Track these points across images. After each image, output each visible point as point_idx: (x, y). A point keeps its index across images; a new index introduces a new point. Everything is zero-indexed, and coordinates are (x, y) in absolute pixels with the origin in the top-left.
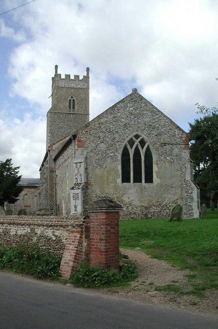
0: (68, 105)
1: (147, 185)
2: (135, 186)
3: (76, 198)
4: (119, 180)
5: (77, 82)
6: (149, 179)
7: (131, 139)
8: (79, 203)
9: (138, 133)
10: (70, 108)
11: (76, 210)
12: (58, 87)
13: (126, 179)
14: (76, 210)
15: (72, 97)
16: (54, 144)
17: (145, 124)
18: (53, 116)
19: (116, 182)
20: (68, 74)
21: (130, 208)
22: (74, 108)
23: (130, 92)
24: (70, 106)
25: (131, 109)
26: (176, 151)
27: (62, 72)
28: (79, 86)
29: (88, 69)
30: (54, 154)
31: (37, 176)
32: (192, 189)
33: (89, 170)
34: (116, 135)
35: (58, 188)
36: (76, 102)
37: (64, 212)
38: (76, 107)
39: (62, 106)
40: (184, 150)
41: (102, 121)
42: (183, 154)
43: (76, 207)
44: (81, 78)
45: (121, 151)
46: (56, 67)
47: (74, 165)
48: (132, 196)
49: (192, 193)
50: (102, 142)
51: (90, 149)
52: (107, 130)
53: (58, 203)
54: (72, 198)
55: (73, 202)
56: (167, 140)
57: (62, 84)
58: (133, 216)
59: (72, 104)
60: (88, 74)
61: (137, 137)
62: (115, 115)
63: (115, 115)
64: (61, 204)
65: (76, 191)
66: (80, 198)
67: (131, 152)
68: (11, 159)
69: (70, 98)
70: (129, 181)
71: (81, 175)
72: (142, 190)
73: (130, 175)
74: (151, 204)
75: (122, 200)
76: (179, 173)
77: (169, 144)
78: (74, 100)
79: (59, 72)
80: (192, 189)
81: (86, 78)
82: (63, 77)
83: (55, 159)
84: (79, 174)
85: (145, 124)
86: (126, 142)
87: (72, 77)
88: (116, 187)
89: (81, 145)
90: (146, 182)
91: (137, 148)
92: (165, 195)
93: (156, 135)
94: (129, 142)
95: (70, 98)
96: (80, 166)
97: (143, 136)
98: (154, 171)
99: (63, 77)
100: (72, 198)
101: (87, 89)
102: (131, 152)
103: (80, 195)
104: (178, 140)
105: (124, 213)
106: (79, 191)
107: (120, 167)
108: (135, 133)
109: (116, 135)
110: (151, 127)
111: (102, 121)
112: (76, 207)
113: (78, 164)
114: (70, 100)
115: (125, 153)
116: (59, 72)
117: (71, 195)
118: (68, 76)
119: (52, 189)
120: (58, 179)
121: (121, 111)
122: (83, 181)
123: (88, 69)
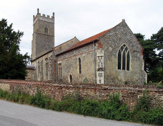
2: (123, 71)
5: (48, 19)
6: (128, 69)
9: (125, 44)
10: (45, 31)
13: (119, 68)
15: (46, 26)
17: (128, 40)
21: (121, 83)
22: (47, 32)
23: (121, 21)
24: (45, 31)
25: (122, 30)
26: (138, 55)
28: (49, 21)
29: (54, 14)
32: (145, 75)
34: (116, 43)
36: (48, 29)
38: (48, 32)
39: (41, 30)
43: (100, 81)
44: (51, 17)
45: (118, 52)
46: (38, 10)
47: (97, 57)
48: (122, 75)
49: (145, 76)
50: (110, 46)
51: (105, 49)
52: (112, 40)
54: (97, 76)
56: (135, 50)
57: (41, 19)
59: (46, 30)
61: (124, 45)
65: (100, 72)
67: (122, 53)
69: (45, 27)
70: (125, 69)
71: (102, 63)
72: (125, 73)
73: (121, 65)
74: (128, 81)
75: (118, 78)
78: (47, 28)
80: (145, 75)
81: (53, 17)
82: (42, 15)
85: (128, 40)
86: (120, 47)
88: (116, 71)
90: (127, 70)
95: (45, 27)
96: (101, 58)
97: (127, 46)
98: (130, 64)
99: (42, 15)
101: (54, 23)
103: (103, 75)
104: (139, 50)
108: (124, 44)
112: (100, 81)
113: (100, 58)
114: (45, 28)
118: (44, 15)
121: (118, 30)
123: (54, 14)
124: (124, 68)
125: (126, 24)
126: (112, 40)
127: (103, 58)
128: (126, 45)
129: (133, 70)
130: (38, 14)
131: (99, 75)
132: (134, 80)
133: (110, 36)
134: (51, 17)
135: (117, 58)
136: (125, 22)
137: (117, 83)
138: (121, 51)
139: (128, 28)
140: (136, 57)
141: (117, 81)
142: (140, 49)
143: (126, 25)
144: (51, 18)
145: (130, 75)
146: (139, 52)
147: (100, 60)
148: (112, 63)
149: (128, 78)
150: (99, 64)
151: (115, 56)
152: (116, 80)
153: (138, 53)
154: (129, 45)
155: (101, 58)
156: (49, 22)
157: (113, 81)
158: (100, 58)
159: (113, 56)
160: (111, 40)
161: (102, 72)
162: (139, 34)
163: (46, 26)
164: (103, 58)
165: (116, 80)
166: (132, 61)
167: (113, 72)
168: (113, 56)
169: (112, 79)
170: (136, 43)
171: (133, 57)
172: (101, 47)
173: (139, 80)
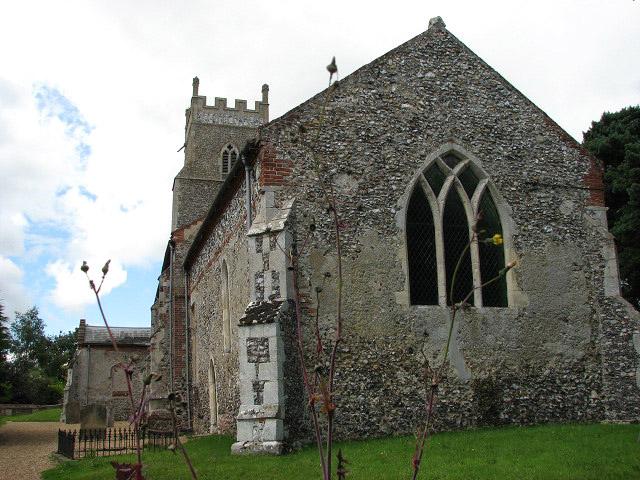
0: (220, 163)
1: (490, 312)
3: (257, 355)
4: (403, 296)
6: (495, 296)
7: (435, 164)
8: (270, 372)
9: (457, 148)
11: (258, 400)
12: (199, 125)
13: (423, 292)
14: (258, 400)
15: (230, 147)
16: (188, 227)
18: (186, 187)
19: (392, 303)
20: (222, 96)
23: (423, 27)
25: (429, 74)
26: (568, 206)
27: (210, 93)
29: (265, 89)
30: (183, 251)
31: (135, 315)
33: (303, 261)
34: (388, 151)
35: (197, 341)
37: (212, 407)
39: (206, 165)
40: (590, 207)
41: (341, 103)
42: (590, 220)
43: (258, 387)
44: (251, 106)
45: (403, 201)
46: (196, 82)
47: (252, 243)
49: (630, 337)
51: (304, 191)
53: (196, 381)
54: (243, 358)
55: (246, 373)
56: (542, 175)
57: (207, 118)
58: (451, 417)
60: (265, 97)
61: (452, 158)
62: (381, 90)
63: (381, 90)
64: (203, 383)
65: (259, 331)
66: (274, 357)
67: (437, 206)
68: (83, 322)
69: (225, 148)
74: (505, 374)
76: (581, 275)
77: (546, 186)
78: (234, 153)
79: (201, 93)
82: (210, 102)
83: (188, 266)
84: (268, 275)
85: (474, 123)
86: (419, 171)
87: (231, 104)
88: (397, 320)
89: (276, 176)
90: (485, 303)
91: (453, 193)
92: (548, 345)
93: (509, 157)
94: (427, 173)
95: (225, 148)
97: (471, 156)
99: (210, 102)
100: (243, 358)
102: (437, 206)
103: (273, 344)
104: (571, 177)
105: (421, 408)
106: (270, 331)
107: (402, 254)
108: (445, 148)
109: (388, 151)
110: (492, 134)
111: (341, 103)
112: (258, 387)
113: (266, 240)
114: (226, 153)
115: (418, 209)
116: (201, 93)
117: (243, 346)
119: (178, 345)
120: (197, 320)
122: (283, 297)
123: (265, 89)
124: (460, 291)
125: (453, 40)
126: (357, 132)
127: (282, 240)
128: (464, 152)
129: (532, 301)
130: (197, 99)
131: (249, 353)
132: (551, 364)
133: (343, 113)
134: (251, 106)
135: (402, 236)
136: (448, 33)
137: (413, 395)
138: (428, 189)
139: (475, 62)
140: (555, 220)
141: (408, 383)
142: (579, 168)
143: (459, 47)
144: (213, 104)
145: (514, 332)
146: (567, 187)
147: (267, 254)
148: (364, 265)
149: (503, 356)
150: (260, 280)
151: (384, 225)
152: (401, 375)
153: (563, 196)
154: (489, 152)
155: (273, 246)
156: (244, 128)
157: (374, 386)
158: (266, 240)
159: (369, 230)
160: (350, 133)
161: (267, 327)
162: (607, 118)
163: (230, 147)
164: (282, 240)
165: (401, 375)
166: (517, 246)
167: (376, 325)
168: (369, 230)
169: (364, 371)
170: (540, 139)
171: (522, 218)
172: (278, 181)
173: (590, 366)
